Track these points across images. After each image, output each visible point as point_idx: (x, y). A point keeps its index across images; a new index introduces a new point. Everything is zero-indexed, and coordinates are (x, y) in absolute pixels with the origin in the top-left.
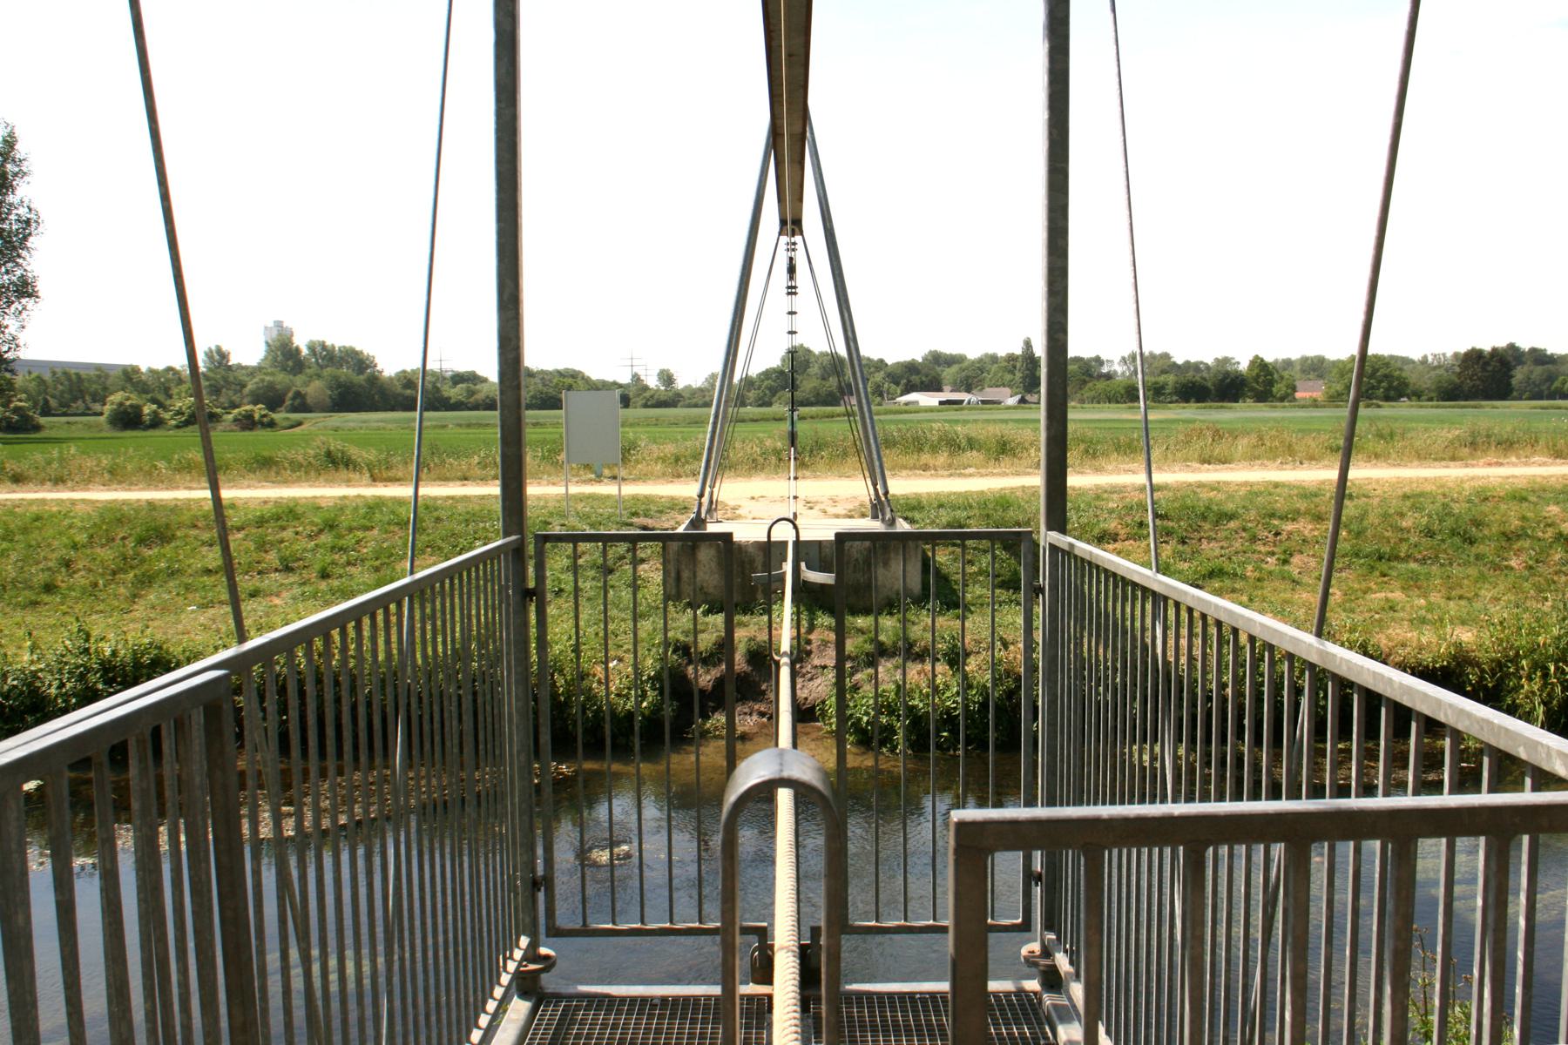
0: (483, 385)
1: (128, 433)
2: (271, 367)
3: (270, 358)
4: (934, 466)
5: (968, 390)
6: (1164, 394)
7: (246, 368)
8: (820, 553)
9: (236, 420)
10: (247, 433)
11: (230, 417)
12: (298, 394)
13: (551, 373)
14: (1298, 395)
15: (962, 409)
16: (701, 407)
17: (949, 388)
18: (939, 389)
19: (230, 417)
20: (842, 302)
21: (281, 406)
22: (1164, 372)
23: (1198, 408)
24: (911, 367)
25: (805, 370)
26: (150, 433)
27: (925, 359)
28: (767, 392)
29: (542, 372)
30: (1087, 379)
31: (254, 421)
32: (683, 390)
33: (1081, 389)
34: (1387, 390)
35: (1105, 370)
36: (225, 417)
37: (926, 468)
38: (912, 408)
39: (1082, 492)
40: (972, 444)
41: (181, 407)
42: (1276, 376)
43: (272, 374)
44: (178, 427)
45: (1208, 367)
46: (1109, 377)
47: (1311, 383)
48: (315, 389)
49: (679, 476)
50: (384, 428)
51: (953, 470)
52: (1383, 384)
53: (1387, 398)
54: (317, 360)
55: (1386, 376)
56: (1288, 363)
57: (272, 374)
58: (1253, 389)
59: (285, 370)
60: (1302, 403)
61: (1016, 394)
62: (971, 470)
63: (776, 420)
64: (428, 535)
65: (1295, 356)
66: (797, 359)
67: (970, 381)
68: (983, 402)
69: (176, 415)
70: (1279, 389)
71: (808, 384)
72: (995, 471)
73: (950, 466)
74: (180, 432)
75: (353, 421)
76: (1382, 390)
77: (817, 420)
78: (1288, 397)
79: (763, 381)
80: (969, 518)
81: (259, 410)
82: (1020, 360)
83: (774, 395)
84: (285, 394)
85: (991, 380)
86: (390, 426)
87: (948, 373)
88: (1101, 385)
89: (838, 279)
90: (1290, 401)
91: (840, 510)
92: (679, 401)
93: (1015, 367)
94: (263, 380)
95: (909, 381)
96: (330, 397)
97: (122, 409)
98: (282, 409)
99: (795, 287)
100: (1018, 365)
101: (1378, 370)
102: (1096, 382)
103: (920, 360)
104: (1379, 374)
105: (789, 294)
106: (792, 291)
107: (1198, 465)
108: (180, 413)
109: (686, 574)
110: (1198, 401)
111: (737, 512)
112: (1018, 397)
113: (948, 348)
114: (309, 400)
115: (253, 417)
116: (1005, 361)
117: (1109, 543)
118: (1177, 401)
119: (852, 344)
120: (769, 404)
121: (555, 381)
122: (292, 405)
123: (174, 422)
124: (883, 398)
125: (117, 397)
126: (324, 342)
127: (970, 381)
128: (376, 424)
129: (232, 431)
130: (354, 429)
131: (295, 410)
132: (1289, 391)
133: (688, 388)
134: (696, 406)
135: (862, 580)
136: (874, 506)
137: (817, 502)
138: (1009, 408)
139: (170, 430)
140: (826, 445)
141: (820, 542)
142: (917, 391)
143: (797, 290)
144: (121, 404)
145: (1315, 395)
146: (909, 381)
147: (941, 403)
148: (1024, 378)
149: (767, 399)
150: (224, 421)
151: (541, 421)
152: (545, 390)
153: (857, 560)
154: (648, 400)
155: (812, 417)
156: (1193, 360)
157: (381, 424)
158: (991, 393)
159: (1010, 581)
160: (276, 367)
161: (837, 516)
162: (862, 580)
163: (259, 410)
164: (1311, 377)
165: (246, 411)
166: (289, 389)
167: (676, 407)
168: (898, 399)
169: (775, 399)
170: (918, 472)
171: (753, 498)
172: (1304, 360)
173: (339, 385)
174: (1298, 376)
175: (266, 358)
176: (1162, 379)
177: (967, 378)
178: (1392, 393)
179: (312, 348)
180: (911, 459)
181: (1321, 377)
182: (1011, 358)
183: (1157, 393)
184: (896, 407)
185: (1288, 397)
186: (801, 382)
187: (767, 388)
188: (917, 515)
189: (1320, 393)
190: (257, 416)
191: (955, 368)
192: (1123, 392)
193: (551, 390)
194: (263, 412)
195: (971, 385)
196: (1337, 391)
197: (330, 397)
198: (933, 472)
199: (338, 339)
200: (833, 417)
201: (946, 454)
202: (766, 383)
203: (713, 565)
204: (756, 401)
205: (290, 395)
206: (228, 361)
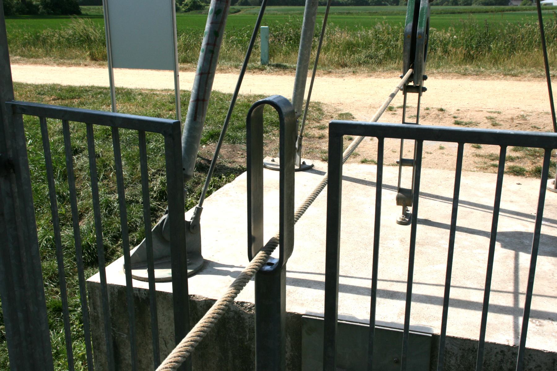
16: (435, 5)
21: (237, 2)
39: (451, 202)
44: (185, 11)
49: (344, 65)
50: (276, 14)
74: (187, 14)
86: (279, 13)
98: (237, 4)
120: (470, 4)
123: (184, 9)
139: (181, 13)
140: (495, 38)
151: (351, 11)
155: (492, 12)
157: (275, 12)
200: (504, 11)
204: (463, 3)
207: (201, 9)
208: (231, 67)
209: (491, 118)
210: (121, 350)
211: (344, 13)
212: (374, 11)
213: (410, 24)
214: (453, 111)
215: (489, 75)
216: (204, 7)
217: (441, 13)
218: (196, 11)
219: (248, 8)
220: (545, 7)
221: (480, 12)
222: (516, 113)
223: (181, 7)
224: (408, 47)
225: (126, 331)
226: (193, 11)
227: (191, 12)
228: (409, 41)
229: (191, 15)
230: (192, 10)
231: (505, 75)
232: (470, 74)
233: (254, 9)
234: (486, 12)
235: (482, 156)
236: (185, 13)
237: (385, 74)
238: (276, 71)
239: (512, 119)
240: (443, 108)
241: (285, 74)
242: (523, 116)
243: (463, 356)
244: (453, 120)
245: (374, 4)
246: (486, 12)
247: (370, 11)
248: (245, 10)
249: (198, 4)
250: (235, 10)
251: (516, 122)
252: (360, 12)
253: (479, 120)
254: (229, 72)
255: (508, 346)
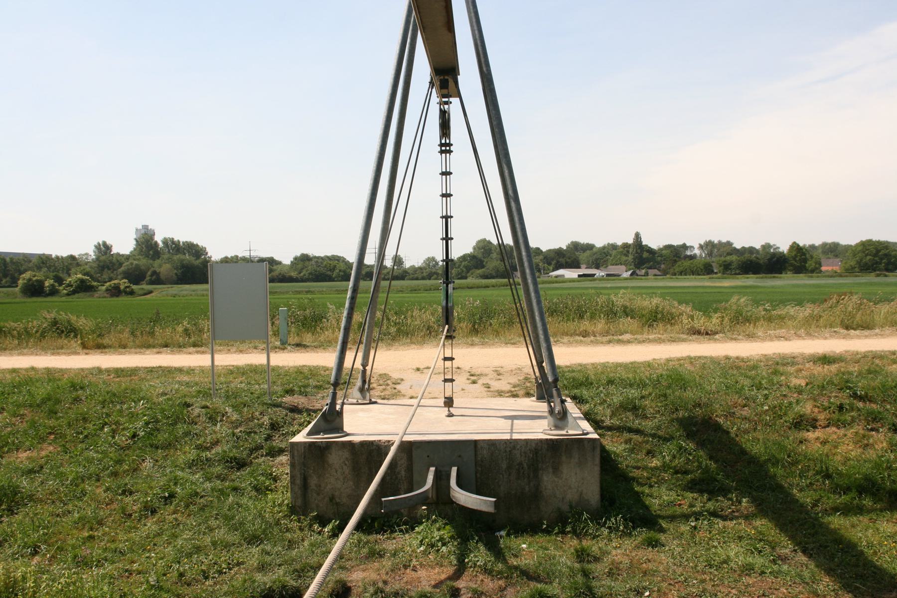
0: (278, 266)
1: (34, 299)
2: (138, 255)
3: (138, 249)
4: (593, 332)
5: (597, 267)
6: (730, 269)
7: (123, 255)
8: (476, 455)
9: (107, 290)
10: (115, 299)
11: (104, 288)
12: (154, 273)
13: (322, 258)
14: (823, 268)
15: (595, 280)
16: (420, 280)
17: (585, 266)
18: (579, 267)
19: (104, 288)
20: (500, 147)
21: (143, 281)
22: (729, 254)
23: (757, 278)
24: (559, 252)
25: (489, 255)
26: (49, 299)
27: (568, 247)
28: (465, 270)
29: (315, 257)
30: (677, 259)
31: (120, 290)
32: (409, 268)
33: (673, 266)
34: (887, 264)
35: (688, 253)
36: (100, 288)
37: (585, 334)
38: (560, 280)
40: (627, 312)
41: (70, 282)
42: (808, 256)
43: (139, 260)
44: (68, 295)
45: (757, 251)
46: (693, 257)
47: (831, 261)
48: (164, 268)
51: (612, 337)
52: (883, 261)
53: (887, 270)
54: (169, 250)
55: (886, 255)
56: (813, 247)
57: (139, 260)
58: (792, 265)
59: (148, 257)
60: (827, 274)
61: (630, 269)
62: (627, 337)
63: (469, 288)
64: (57, 419)
65: (818, 242)
66: (484, 247)
67: (598, 262)
68: (608, 275)
69: (67, 287)
70: (810, 264)
71: (493, 263)
72: (650, 337)
73: (607, 333)
74: (70, 299)
75: (186, 290)
76: (883, 265)
77: (496, 288)
78: (816, 270)
79: (461, 262)
80: (643, 397)
81: (123, 283)
82: (632, 247)
83: (468, 272)
84: (146, 273)
85: (612, 260)
87: (583, 256)
88: (687, 263)
89: (496, 130)
90: (817, 273)
91: (504, 385)
92: (406, 276)
93: (628, 252)
94: (132, 264)
95: (558, 262)
96: (176, 274)
97: (31, 282)
98: (144, 282)
99: (450, 145)
100: (631, 250)
101: (880, 251)
102: (683, 261)
103: (565, 248)
104: (880, 254)
105: (442, 152)
106: (446, 149)
107: (845, 331)
108: (70, 285)
109: (313, 482)
110: (754, 273)
111: (398, 387)
112: (630, 273)
113: (583, 240)
114: (162, 277)
115: (120, 288)
116: (622, 247)
117: (808, 431)
118: (739, 274)
119: (513, 204)
120: (466, 278)
121: (325, 263)
122: (150, 280)
123: (65, 292)
124: (541, 273)
125: (27, 275)
126: (173, 239)
127: (598, 262)
128: (202, 292)
129: (105, 297)
130: (187, 296)
131: (152, 283)
132: (817, 266)
133: (413, 267)
134: (417, 279)
135: (527, 489)
136: (539, 386)
137: (480, 375)
138: (626, 279)
141: (476, 442)
142: (563, 268)
143: (452, 148)
144: (30, 280)
145: (835, 268)
146: (558, 262)
147: (579, 276)
148: (634, 259)
149: (464, 274)
150: (99, 290)
152: (318, 269)
153: (520, 464)
154: (385, 275)
156: (747, 246)
158: (613, 270)
159: (702, 481)
160: (142, 255)
161: (500, 394)
162: (527, 489)
163: (123, 283)
164: (830, 256)
165: (115, 284)
166: (149, 269)
167: (404, 279)
168: (551, 274)
169: (468, 275)
170: (577, 338)
171: (418, 369)
172: (824, 245)
173: (183, 266)
174: (821, 256)
175: (135, 249)
176: (728, 258)
177: (597, 259)
178: (890, 267)
179: (165, 242)
180: (572, 326)
181: (836, 256)
182: (626, 246)
183: (727, 269)
184: (550, 279)
185: (816, 270)
186: (487, 262)
187: (464, 266)
188: (585, 393)
189: (838, 267)
190: (122, 287)
191: (588, 253)
192: (702, 268)
193: (322, 269)
194: (126, 285)
195: (599, 264)
196: (851, 266)
197: (176, 274)
198: (592, 338)
199: (182, 237)
201: (603, 321)
202: (463, 263)
203: (347, 470)
205: (149, 273)
206: (111, 251)
207: (92, 291)
208: (249, 348)
209: (496, 371)
210: (309, 481)
211: (302, 292)
212: (342, 289)
213: (445, 302)
214: (467, 369)
215: (493, 345)
216: (97, 288)
217: (430, 289)
218: (85, 293)
219: (164, 288)
220: (555, 279)
221: (478, 287)
222: (514, 367)
223: (61, 288)
224: (445, 314)
225: (312, 468)
226: (80, 294)
227: (77, 295)
228: (445, 311)
229: (77, 300)
230: (78, 292)
231: (506, 344)
232: (476, 345)
233: (173, 289)
234: (487, 287)
235: (492, 391)
236: (67, 297)
237: (402, 347)
238: (298, 350)
239: (512, 371)
240: (460, 367)
241: (308, 352)
242: (519, 368)
243: (489, 448)
244: (469, 374)
245: (340, 279)
246: (487, 287)
247: (339, 289)
248: (160, 290)
249: (88, 284)
250: (145, 292)
251: (514, 372)
252: (324, 290)
253: (487, 372)
254: (251, 353)
255: (507, 440)
